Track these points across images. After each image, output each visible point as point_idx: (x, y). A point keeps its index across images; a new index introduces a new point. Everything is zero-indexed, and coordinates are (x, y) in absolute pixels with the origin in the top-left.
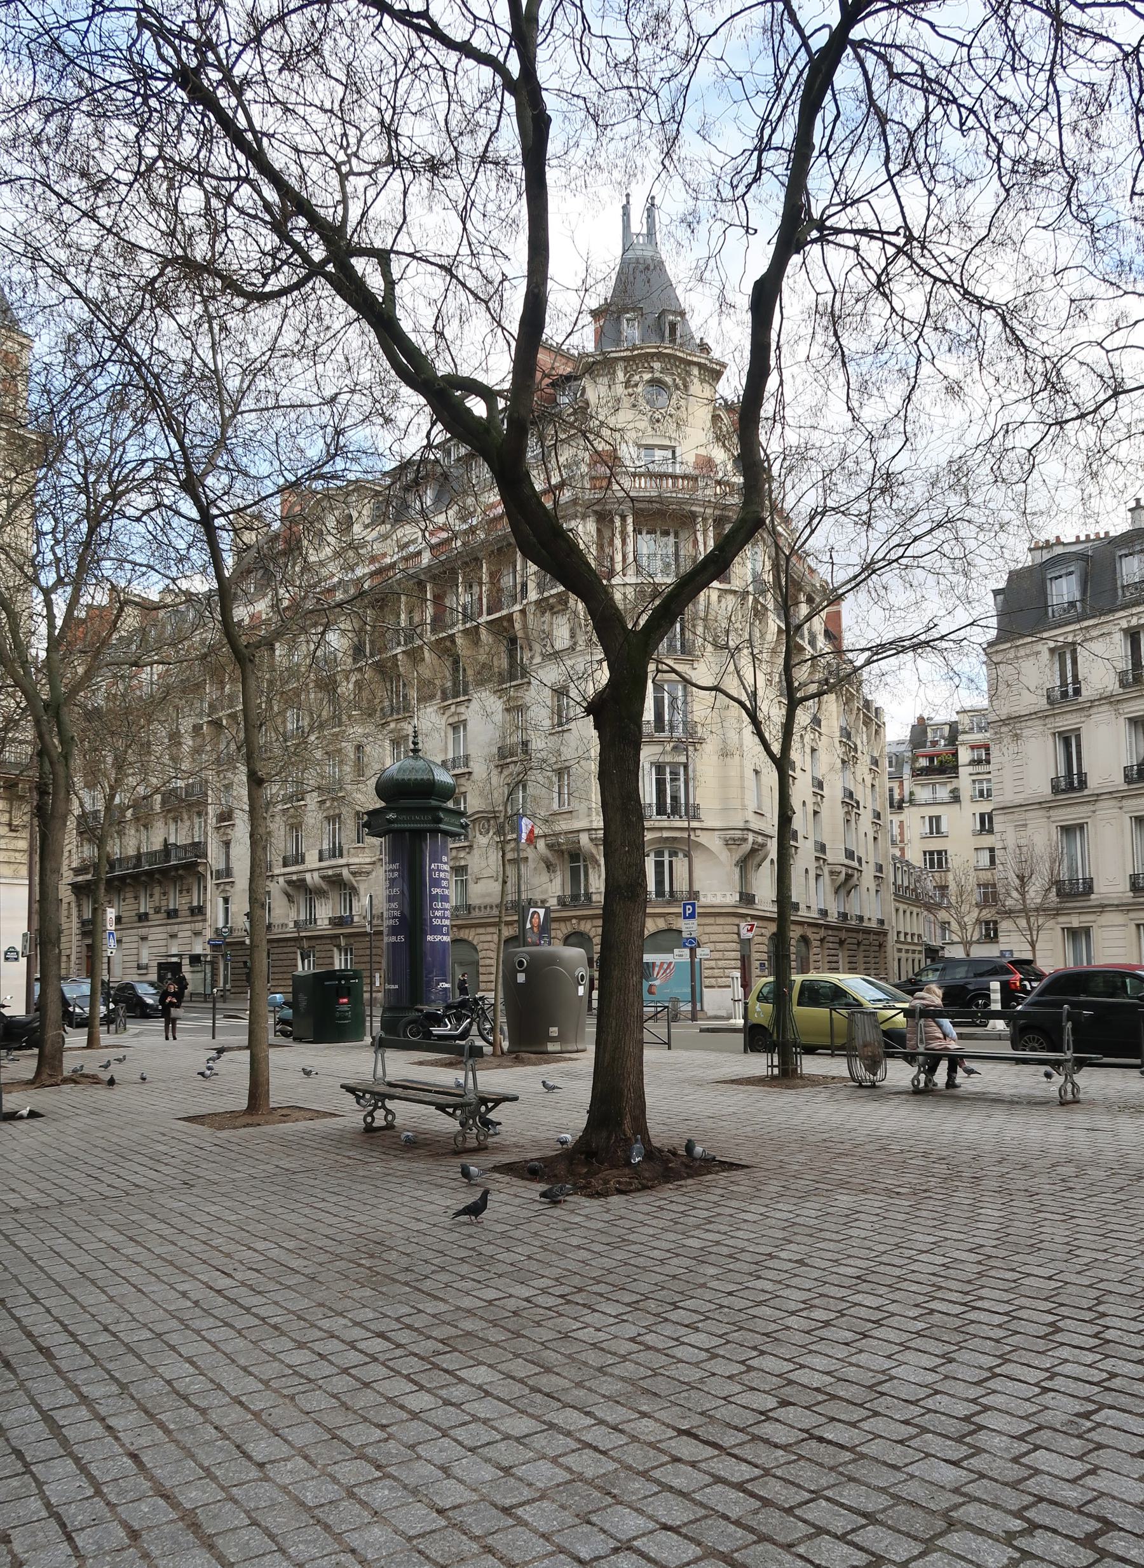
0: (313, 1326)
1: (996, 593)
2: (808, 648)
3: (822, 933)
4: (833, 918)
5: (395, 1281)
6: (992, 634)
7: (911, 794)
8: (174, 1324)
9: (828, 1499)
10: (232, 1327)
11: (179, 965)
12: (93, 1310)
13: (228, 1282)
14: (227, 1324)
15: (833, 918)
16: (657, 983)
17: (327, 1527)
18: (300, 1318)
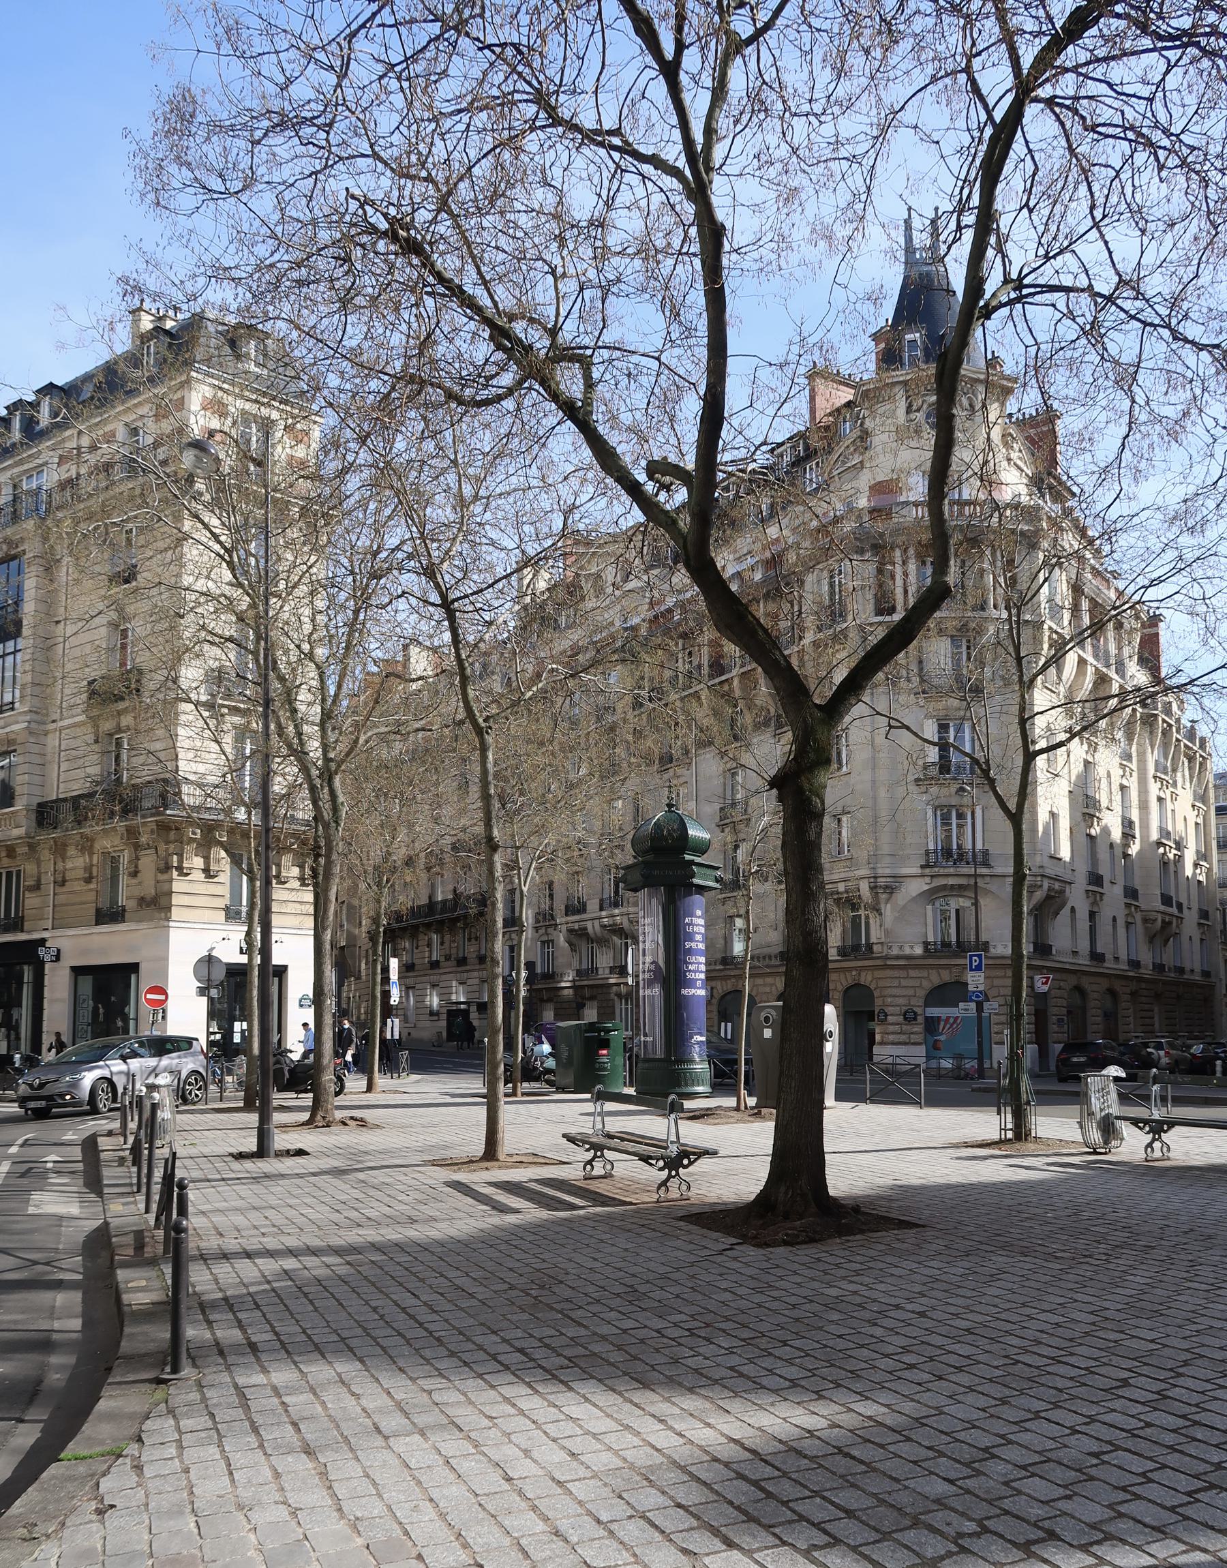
0: (469, 1340)
2: (1115, 676)
4: (1147, 971)
5: (553, 1309)
8: (359, 1331)
9: (824, 1498)
10: (404, 1337)
11: (467, 1012)
12: (298, 1317)
13: (414, 1301)
14: (400, 1334)
15: (1147, 971)
16: (942, 1038)
17: (419, 1483)
18: (461, 1333)
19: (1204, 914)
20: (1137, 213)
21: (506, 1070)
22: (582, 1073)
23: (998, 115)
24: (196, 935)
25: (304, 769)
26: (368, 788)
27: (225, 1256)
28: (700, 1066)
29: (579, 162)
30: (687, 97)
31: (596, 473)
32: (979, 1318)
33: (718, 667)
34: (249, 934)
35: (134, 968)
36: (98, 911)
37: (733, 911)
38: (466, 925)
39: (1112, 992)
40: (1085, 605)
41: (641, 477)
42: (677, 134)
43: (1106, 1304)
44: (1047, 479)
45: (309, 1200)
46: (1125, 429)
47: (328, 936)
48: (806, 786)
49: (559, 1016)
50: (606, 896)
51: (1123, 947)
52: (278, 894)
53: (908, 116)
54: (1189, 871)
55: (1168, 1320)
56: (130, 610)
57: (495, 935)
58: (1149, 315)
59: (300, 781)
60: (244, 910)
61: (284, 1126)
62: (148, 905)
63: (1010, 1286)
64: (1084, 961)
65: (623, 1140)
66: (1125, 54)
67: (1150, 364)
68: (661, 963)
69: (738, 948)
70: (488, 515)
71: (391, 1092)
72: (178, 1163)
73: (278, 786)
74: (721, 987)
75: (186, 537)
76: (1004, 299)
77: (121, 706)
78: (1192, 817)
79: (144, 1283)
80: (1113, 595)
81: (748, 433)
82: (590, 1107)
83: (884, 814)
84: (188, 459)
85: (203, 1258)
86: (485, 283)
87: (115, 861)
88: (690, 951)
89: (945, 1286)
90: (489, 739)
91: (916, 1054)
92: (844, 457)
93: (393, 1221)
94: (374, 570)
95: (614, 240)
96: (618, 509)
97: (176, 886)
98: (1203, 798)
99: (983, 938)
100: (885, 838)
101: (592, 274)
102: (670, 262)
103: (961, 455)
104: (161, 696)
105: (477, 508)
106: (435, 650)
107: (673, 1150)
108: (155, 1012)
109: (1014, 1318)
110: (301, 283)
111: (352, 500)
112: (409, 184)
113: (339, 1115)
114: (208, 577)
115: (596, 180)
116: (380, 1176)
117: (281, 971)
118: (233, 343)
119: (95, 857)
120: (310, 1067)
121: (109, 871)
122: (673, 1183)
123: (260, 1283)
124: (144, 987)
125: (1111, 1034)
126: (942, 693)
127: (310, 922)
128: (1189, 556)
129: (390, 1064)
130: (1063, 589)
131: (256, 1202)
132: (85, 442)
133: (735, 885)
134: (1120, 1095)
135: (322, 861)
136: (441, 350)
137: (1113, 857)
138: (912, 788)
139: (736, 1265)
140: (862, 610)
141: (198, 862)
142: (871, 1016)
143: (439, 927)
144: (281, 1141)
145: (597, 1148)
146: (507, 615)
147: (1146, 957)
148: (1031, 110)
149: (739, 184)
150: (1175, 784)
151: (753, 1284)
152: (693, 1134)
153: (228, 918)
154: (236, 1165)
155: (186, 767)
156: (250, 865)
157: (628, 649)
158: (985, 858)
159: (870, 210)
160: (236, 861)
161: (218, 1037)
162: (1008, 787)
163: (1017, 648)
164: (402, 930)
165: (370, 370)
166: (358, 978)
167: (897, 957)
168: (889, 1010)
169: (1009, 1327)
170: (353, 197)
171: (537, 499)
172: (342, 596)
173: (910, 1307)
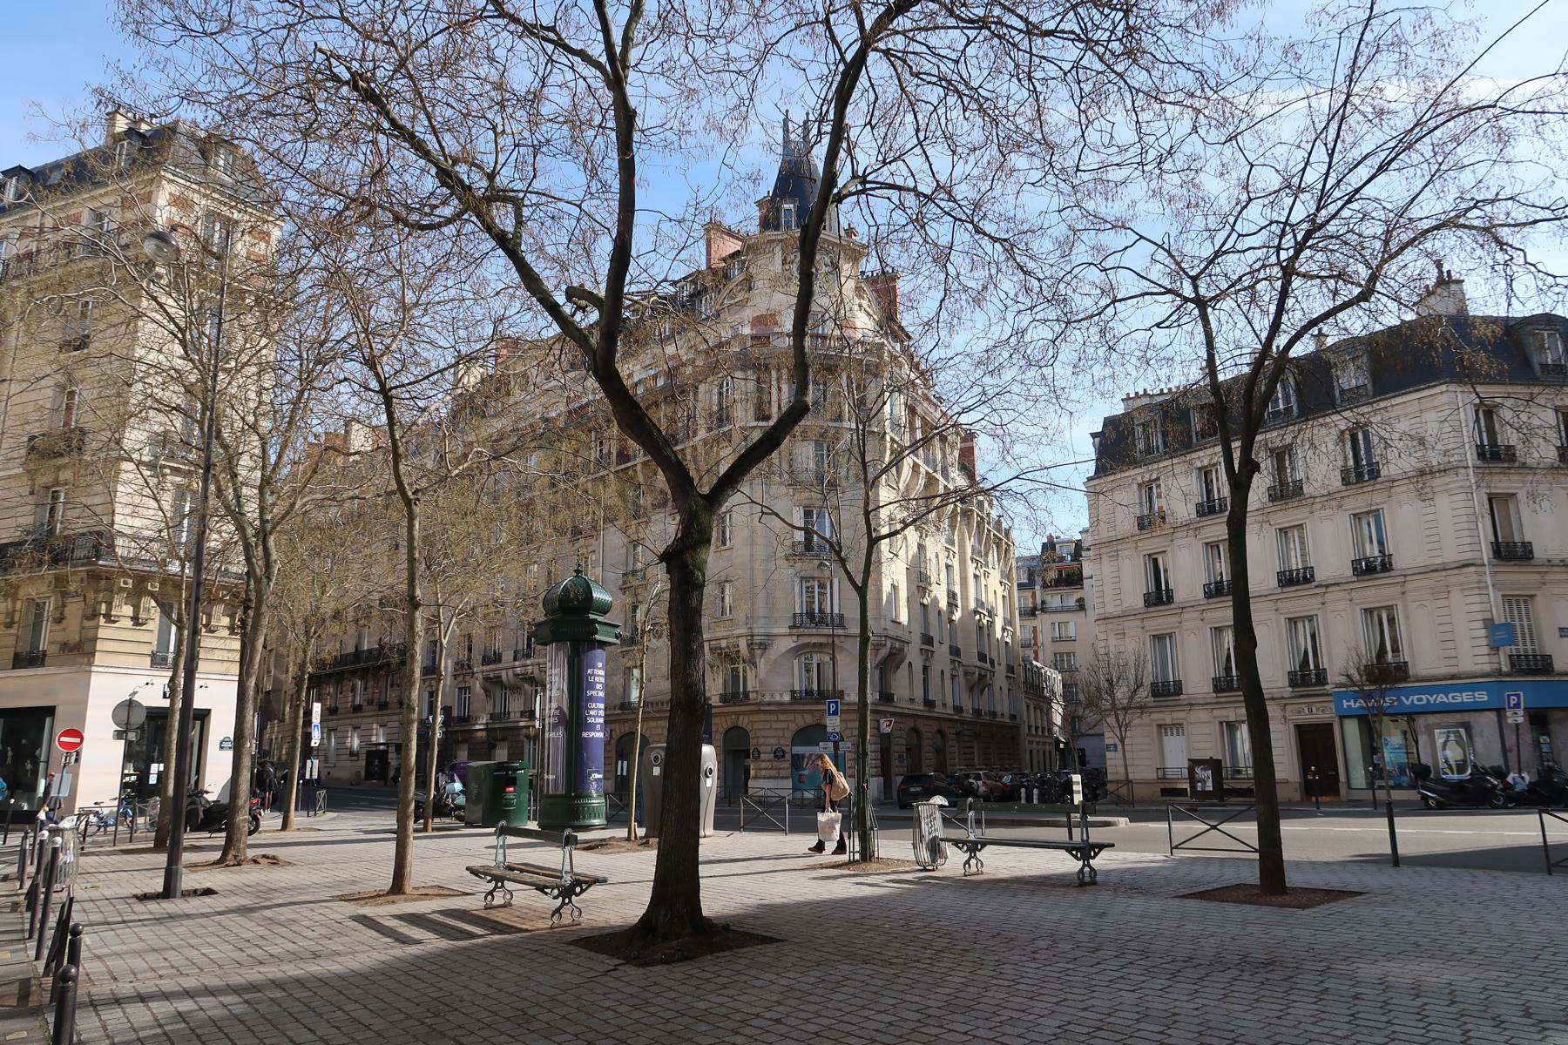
1: (1094, 435)
3: (958, 727)
4: (968, 715)
5: (445, 1036)
6: (1091, 468)
7: (1043, 602)
11: (385, 753)
15: (968, 715)
19: (1010, 669)
20: (949, 138)
21: (417, 807)
22: (491, 809)
23: (849, 56)
24: (124, 674)
25: (241, 528)
26: (302, 549)
27: (117, 1001)
28: (597, 801)
29: (521, 46)
30: (609, 11)
31: (522, 292)
32: (825, 1022)
33: (623, 456)
34: (172, 679)
35: (50, 711)
36: (16, 655)
37: (630, 663)
38: (388, 673)
39: (940, 732)
40: (918, 423)
41: (560, 298)
42: (600, 36)
43: (930, 1003)
44: (888, 321)
45: (212, 940)
46: (942, 294)
47: (252, 682)
48: (690, 561)
49: (472, 757)
50: (520, 647)
51: (949, 695)
52: (206, 641)
53: (782, 47)
54: (999, 634)
55: (978, 1014)
56: (78, 374)
57: (412, 684)
58: (958, 213)
59: (236, 538)
60: (171, 656)
61: (194, 866)
62: (71, 650)
63: (851, 991)
64: (919, 706)
65: (522, 871)
66: (936, 28)
67: (960, 248)
68: (566, 709)
69: (635, 695)
70: (426, 319)
71: (306, 830)
72: (75, 907)
73: (214, 542)
74: (619, 730)
75: (139, 316)
76: (853, 189)
77: (60, 461)
78: (1000, 590)
79: (25, 1034)
80: (938, 415)
81: (651, 271)
82: (493, 840)
83: (760, 583)
84: (149, 247)
85: (93, 1004)
86: (435, 132)
87: (39, 607)
88: (591, 699)
89: (799, 995)
90: (417, 510)
91: (784, 787)
92: (731, 295)
93: (296, 957)
94: (321, 356)
95: (547, 109)
96: (542, 323)
97: (101, 633)
98: (1008, 577)
99: (839, 687)
100: (760, 603)
101: (526, 134)
102: (592, 133)
103: (820, 302)
104: (103, 455)
105: (416, 312)
106: (374, 428)
107: (568, 879)
108: (68, 755)
109: (855, 1020)
110: (269, 113)
111: (303, 297)
112: (372, 46)
113: (251, 853)
114: (160, 351)
115: (534, 62)
116: (288, 913)
117: (204, 715)
118: (204, 154)
119: (19, 604)
120: (225, 807)
121: (32, 618)
122: (566, 910)
123: (151, 1028)
124: (58, 731)
125: (941, 767)
126: (808, 487)
127: (235, 669)
128: (991, 392)
129: (308, 804)
130: (902, 413)
131: (157, 944)
132: (49, 222)
133: (632, 641)
134: (944, 819)
135: (251, 613)
136: (392, 181)
137: (940, 621)
138: (783, 563)
139: (618, 985)
140: (743, 416)
141: (128, 610)
142: (747, 754)
143: (364, 674)
144: (188, 881)
145: (498, 879)
146: (440, 405)
147: (967, 704)
148: (872, 57)
149: (650, 80)
150: (987, 565)
151: (632, 1001)
152: (586, 863)
153: (153, 664)
154: (139, 907)
155: (123, 521)
156: (179, 615)
157: (547, 436)
158: (841, 621)
159: (752, 112)
160: (166, 610)
161: (133, 778)
162: (856, 566)
163: (863, 455)
164: (327, 677)
165: (326, 190)
166: (282, 720)
167: (769, 704)
168: (762, 749)
169: (849, 1028)
170: (321, 51)
171: (468, 310)
172: (288, 378)
173: (768, 1015)
